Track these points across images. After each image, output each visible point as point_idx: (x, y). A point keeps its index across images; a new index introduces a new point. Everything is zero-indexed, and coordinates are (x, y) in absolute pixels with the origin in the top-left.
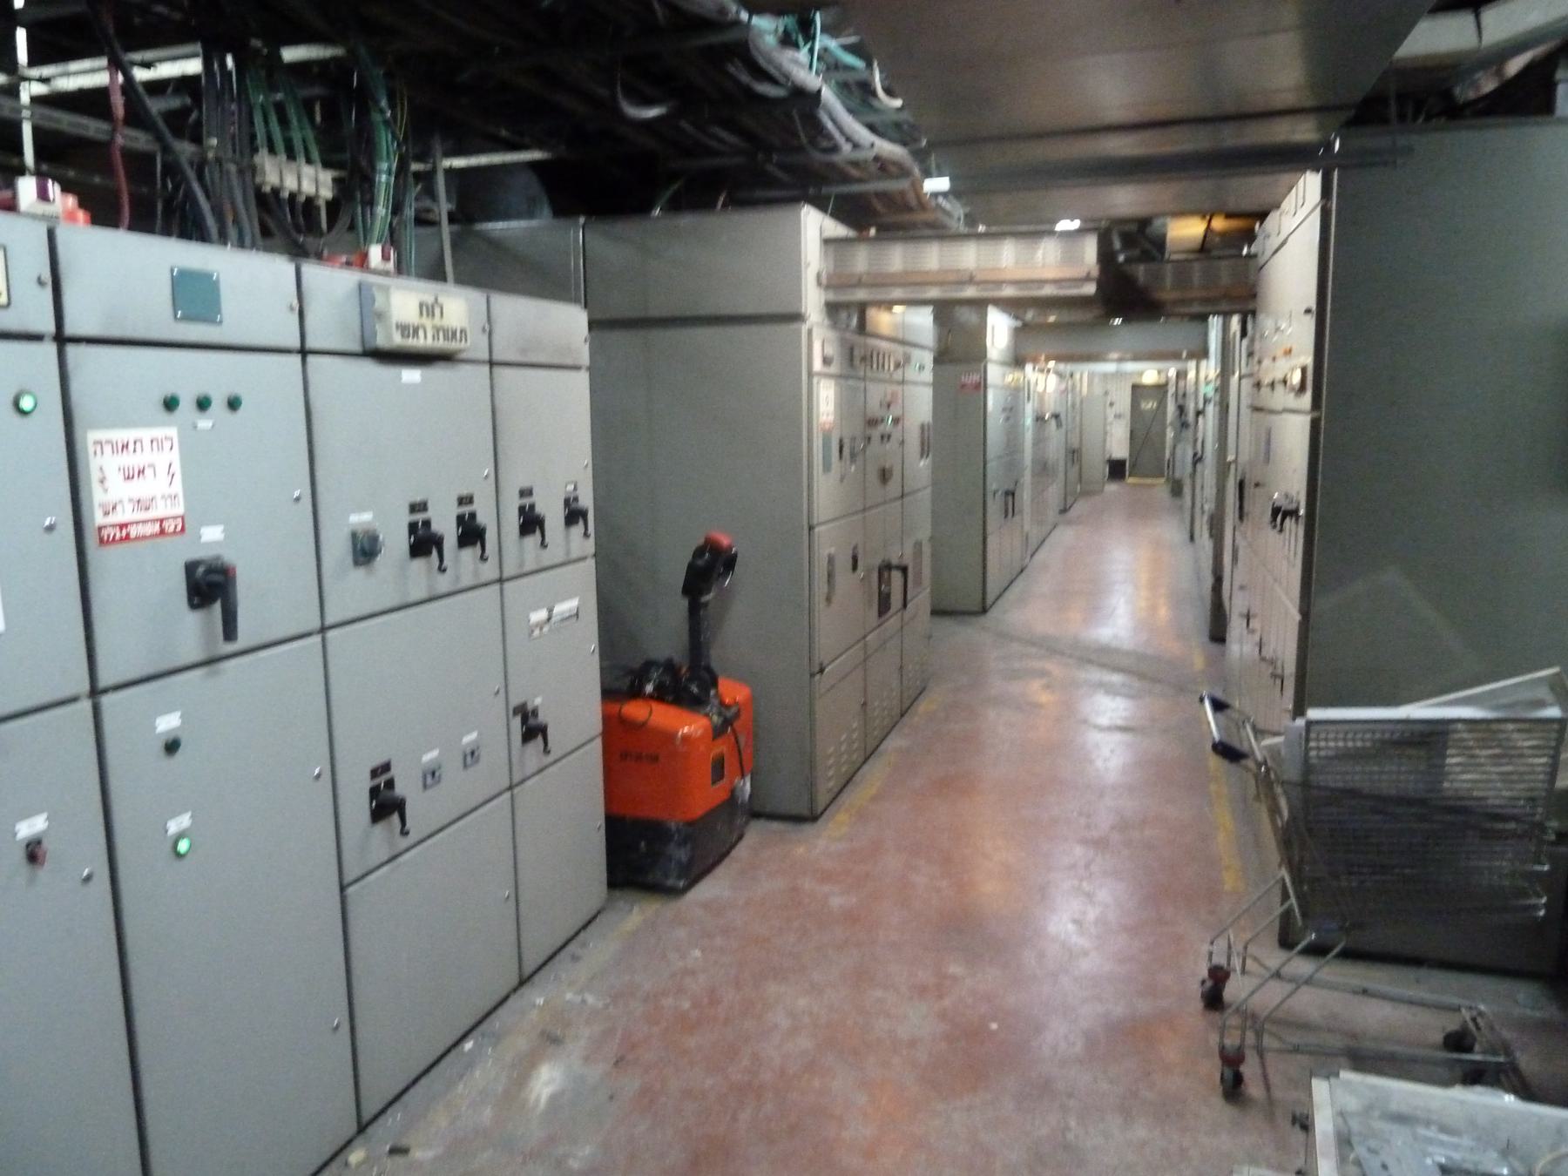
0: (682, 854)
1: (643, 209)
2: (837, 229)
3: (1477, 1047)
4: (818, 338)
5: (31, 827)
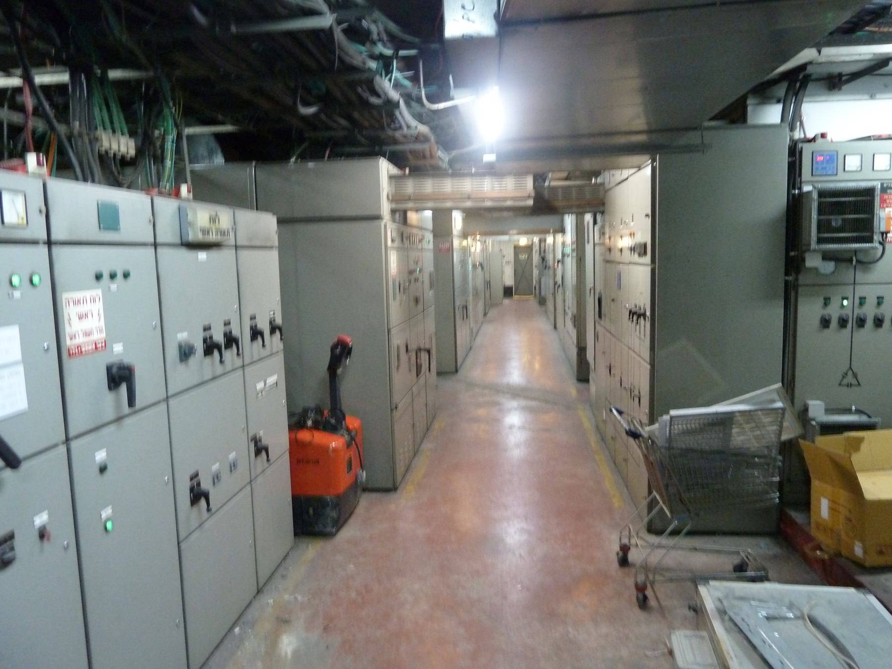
0: (334, 514)
1: (285, 158)
2: (394, 170)
3: (749, 568)
4: (388, 228)
5: (41, 519)
